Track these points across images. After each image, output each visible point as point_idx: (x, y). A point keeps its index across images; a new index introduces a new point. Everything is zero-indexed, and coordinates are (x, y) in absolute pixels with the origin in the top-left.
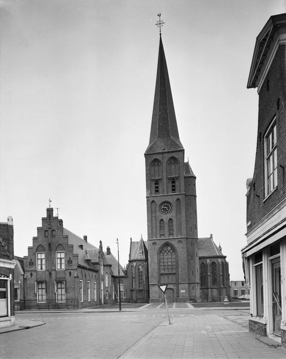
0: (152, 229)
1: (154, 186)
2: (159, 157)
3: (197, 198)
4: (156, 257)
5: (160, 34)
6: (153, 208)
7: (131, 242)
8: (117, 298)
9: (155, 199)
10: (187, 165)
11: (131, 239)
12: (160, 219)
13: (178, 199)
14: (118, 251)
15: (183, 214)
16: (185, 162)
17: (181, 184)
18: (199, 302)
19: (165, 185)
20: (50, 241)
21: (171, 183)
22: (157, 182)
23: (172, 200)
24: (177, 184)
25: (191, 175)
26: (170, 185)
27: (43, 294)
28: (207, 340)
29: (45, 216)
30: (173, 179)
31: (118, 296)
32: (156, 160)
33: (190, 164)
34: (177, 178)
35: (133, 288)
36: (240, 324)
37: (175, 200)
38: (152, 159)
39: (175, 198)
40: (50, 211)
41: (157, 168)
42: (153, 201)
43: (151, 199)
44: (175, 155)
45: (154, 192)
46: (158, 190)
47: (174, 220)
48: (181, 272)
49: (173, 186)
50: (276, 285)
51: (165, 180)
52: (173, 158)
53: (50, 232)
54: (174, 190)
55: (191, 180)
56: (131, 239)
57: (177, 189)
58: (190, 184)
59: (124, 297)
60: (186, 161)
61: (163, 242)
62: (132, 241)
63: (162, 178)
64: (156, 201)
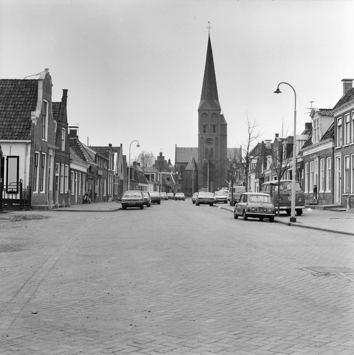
0: (201, 153)
2: (207, 112)
3: (227, 136)
5: (209, 34)
7: (176, 148)
9: (203, 136)
10: (222, 116)
11: (176, 145)
13: (216, 137)
15: (219, 146)
16: (221, 114)
17: (218, 128)
18: (250, 198)
19: (209, 128)
20: (161, 167)
21: (213, 128)
23: (213, 138)
24: (216, 128)
25: (224, 123)
26: (212, 128)
29: (159, 155)
32: (204, 113)
33: (224, 115)
34: (217, 125)
35: (187, 186)
37: (215, 138)
38: (202, 112)
39: (215, 136)
40: (161, 154)
43: (201, 136)
44: (216, 112)
45: (202, 132)
47: (214, 149)
49: (214, 129)
50: (309, 180)
51: (209, 126)
52: (214, 113)
53: (161, 163)
54: (214, 132)
55: (224, 126)
56: (176, 145)
57: (216, 131)
60: (221, 113)
62: (177, 147)
64: (204, 137)
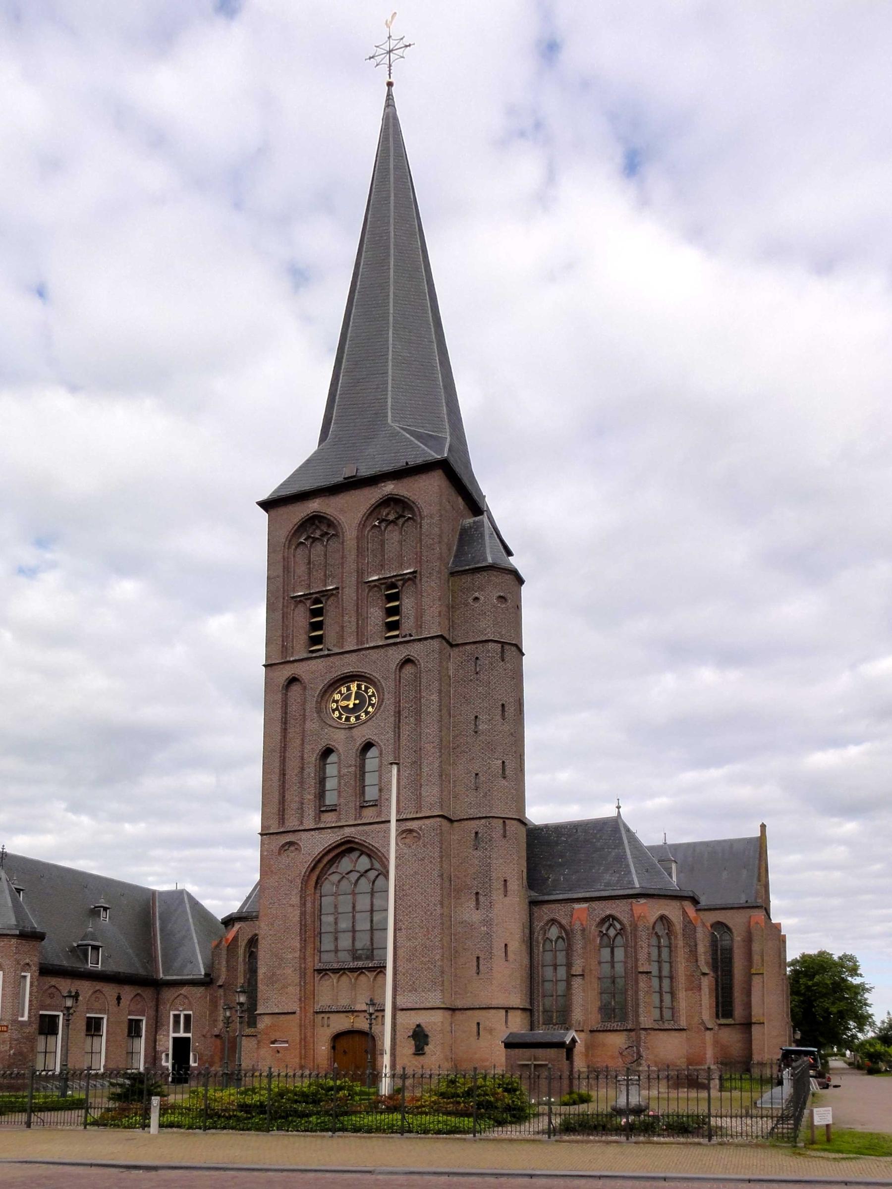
1: (301, 618)
4: (295, 900)
6: (294, 708)
8: (164, 1064)
12: (320, 747)
14: (846, 1183)
19: (356, 620)
22: (317, 606)
27: (43, 1055)
28: (656, 998)
30: (393, 586)
31: (167, 1055)
36: (125, 564)
39: (397, 655)
41: (319, 548)
42: (293, 680)
46: (321, 636)
48: (409, 960)
51: (349, 594)
58: (476, 599)
59: (195, 1062)
61: (330, 839)
63: (339, 585)
